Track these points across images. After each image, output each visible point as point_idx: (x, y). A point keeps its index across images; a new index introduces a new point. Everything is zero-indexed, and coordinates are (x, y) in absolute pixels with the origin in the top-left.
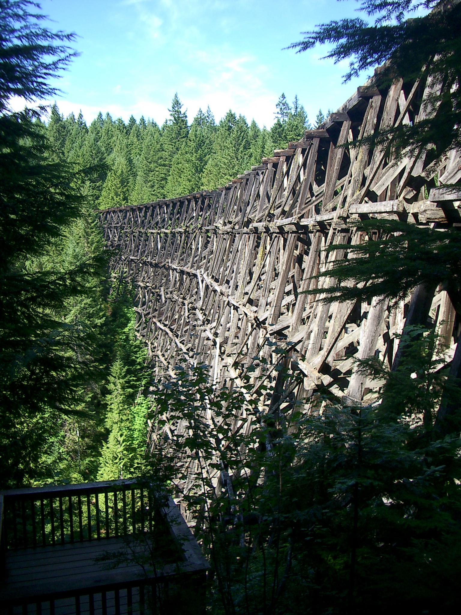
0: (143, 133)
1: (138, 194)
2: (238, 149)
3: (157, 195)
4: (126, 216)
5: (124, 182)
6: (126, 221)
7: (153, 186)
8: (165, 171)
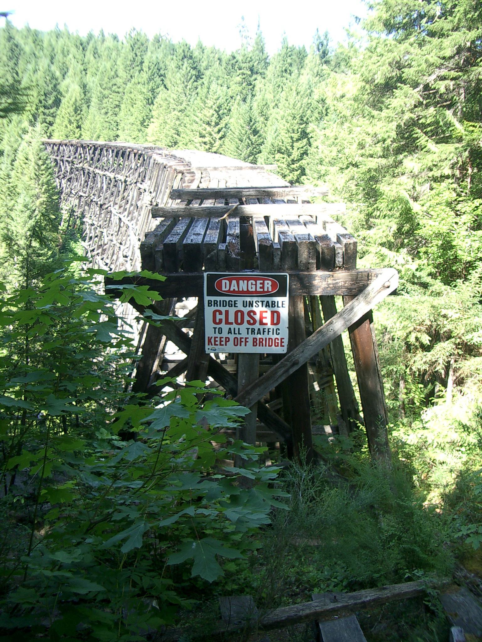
0: (101, 49)
1: (91, 124)
2: (186, 86)
3: (110, 123)
4: (77, 150)
5: (77, 110)
6: (77, 155)
7: (107, 113)
8: (119, 99)
